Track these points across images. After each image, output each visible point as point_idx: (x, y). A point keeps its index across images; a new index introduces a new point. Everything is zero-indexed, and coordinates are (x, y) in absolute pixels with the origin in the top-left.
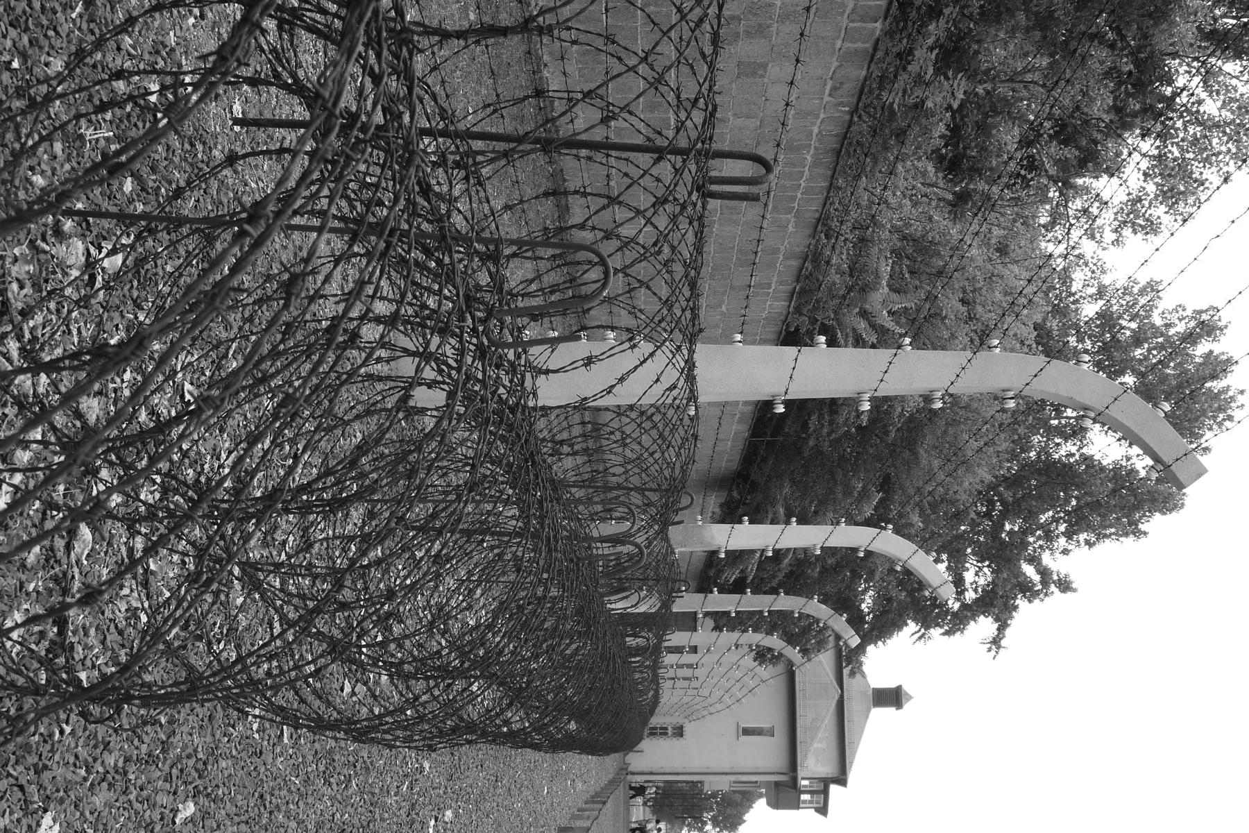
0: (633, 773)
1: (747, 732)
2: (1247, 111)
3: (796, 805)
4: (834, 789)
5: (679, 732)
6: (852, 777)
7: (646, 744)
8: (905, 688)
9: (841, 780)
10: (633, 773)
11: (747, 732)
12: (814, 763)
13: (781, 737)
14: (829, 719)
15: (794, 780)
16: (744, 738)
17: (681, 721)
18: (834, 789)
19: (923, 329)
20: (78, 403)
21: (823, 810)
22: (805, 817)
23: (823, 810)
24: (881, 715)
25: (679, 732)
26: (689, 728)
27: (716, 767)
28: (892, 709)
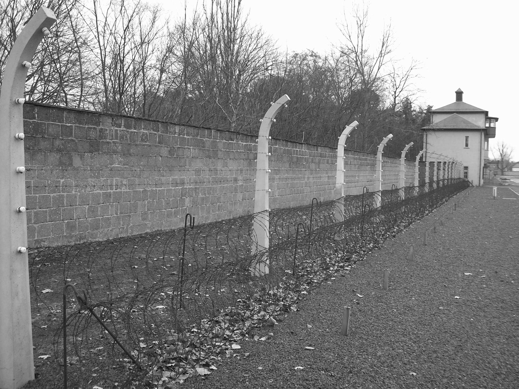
0: (480, 184)
1: (467, 145)
2: (447, 388)
3: (494, 128)
4: (490, 115)
5: (466, 168)
6: (485, 109)
7: (470, 179)
8: (456, 90)
9: (486, 113)
10: (480, 184)
11: (467, 145)
12: (480, 122)
13: (470, 134)
14: (465, 117)
15: (483, 130)
16: (469, 147)
17: (462, 167)
18: (490, 115)
19: (346, 163)
20: (414, 111)
21: (496, 119)
22: (498, 126)
23: (496, 119)
24: (465, 99)
25: (466, 168)
26: (466, 165)
27: (477, 156)
28: (463, 95)
